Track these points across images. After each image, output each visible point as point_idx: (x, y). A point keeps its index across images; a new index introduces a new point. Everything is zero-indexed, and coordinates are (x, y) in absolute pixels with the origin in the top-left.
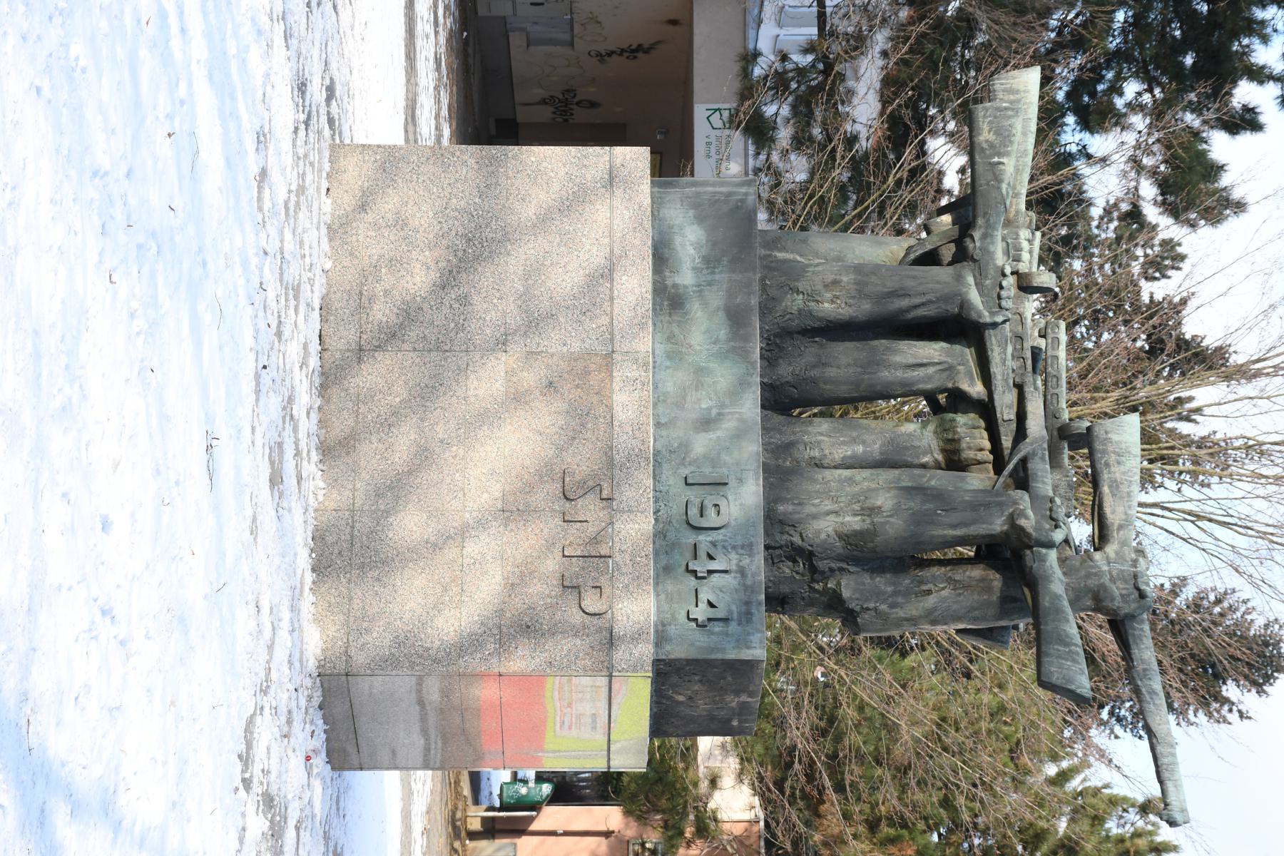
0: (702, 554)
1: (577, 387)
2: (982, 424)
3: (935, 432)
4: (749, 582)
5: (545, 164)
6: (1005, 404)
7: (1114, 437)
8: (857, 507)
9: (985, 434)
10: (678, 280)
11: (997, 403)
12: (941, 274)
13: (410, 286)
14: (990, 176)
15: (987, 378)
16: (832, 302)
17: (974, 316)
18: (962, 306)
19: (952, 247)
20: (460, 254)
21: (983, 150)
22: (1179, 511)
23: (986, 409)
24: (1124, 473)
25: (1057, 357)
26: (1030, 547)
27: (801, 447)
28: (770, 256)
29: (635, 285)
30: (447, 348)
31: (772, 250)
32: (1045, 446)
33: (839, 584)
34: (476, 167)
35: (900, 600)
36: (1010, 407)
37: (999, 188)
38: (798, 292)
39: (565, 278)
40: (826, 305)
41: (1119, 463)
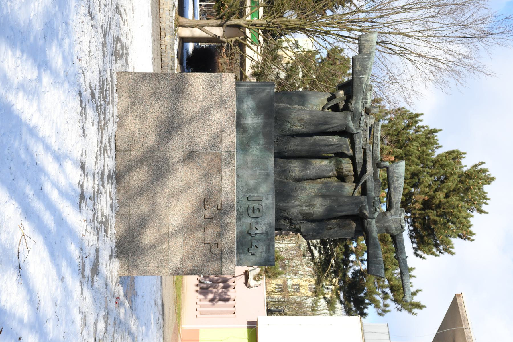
0: (253, 228)
1: (209, 165)
2: (351, 162)
3: (334, 164)
4: (269, 237)
5: (197, 80)
6: (359, 156)
7: (396, 171)
8: (307, 204)
9: (352, 166)
10: (246, 122)
11: (356, 157)
12: (339, 115)
13: (148, 127)
14: (359, 82)
15: (354, 149)
16: (301, 126)
17: (350, 131)
18: (346, 128)
19: (344, 103)
20: (166, 115)
21: (357, 73)
22: (397, 46)
23: (353, 159)
24: (399, 184)
25: (377, 136)
26: (367, 219)
27: (288, 172)
28: (278, 106)
29: (230, 138)
30: (162, 150)
31: (279, 103)
32: (373, 175)
33: (300, 227)
34: (171, 81)
35: (321, 231)
36: (360, 158)
37: (362, 86)
38: (288, 122)
39: (204, 138)
40: (298, 127)
41: (397, 180)
